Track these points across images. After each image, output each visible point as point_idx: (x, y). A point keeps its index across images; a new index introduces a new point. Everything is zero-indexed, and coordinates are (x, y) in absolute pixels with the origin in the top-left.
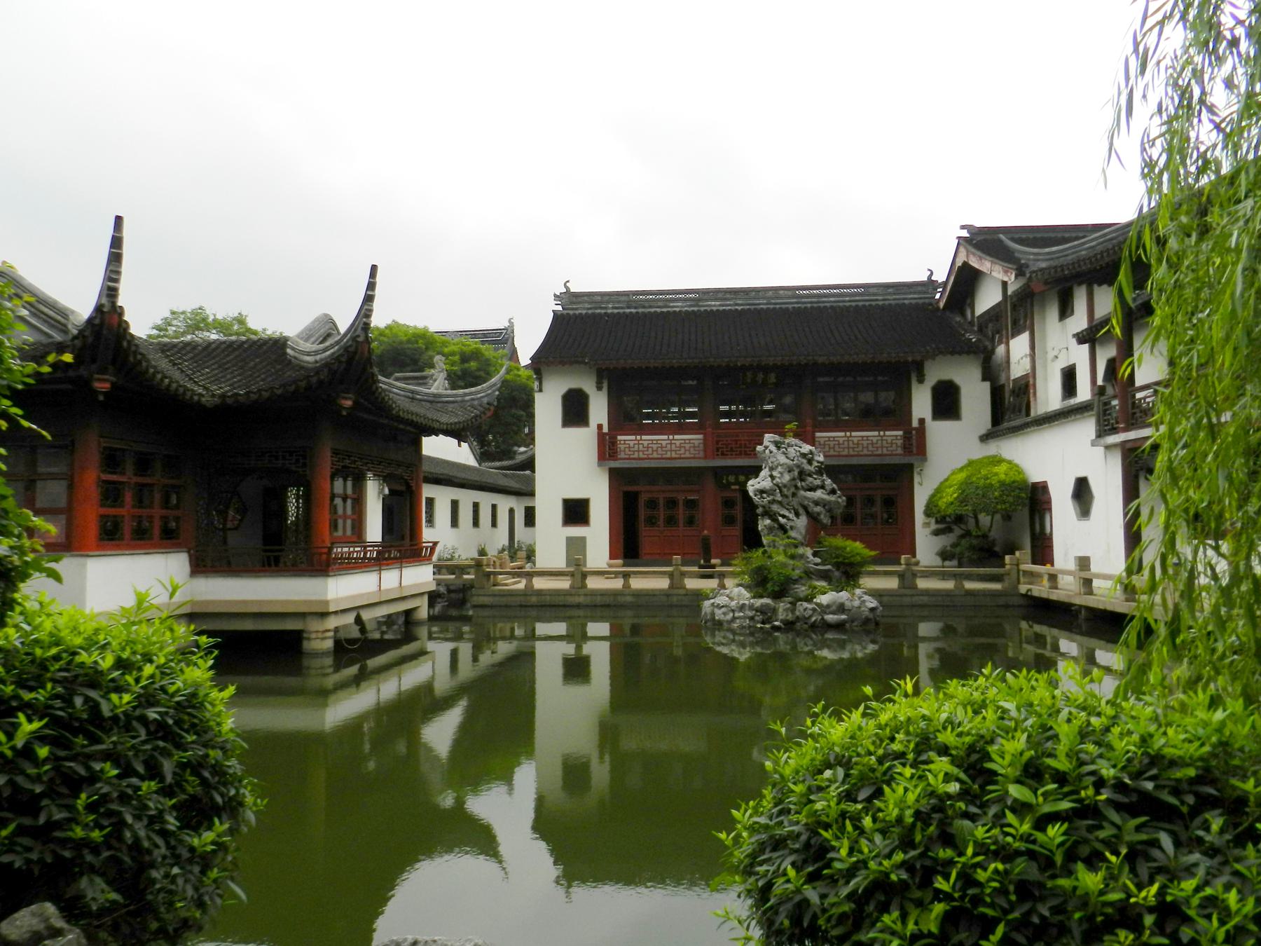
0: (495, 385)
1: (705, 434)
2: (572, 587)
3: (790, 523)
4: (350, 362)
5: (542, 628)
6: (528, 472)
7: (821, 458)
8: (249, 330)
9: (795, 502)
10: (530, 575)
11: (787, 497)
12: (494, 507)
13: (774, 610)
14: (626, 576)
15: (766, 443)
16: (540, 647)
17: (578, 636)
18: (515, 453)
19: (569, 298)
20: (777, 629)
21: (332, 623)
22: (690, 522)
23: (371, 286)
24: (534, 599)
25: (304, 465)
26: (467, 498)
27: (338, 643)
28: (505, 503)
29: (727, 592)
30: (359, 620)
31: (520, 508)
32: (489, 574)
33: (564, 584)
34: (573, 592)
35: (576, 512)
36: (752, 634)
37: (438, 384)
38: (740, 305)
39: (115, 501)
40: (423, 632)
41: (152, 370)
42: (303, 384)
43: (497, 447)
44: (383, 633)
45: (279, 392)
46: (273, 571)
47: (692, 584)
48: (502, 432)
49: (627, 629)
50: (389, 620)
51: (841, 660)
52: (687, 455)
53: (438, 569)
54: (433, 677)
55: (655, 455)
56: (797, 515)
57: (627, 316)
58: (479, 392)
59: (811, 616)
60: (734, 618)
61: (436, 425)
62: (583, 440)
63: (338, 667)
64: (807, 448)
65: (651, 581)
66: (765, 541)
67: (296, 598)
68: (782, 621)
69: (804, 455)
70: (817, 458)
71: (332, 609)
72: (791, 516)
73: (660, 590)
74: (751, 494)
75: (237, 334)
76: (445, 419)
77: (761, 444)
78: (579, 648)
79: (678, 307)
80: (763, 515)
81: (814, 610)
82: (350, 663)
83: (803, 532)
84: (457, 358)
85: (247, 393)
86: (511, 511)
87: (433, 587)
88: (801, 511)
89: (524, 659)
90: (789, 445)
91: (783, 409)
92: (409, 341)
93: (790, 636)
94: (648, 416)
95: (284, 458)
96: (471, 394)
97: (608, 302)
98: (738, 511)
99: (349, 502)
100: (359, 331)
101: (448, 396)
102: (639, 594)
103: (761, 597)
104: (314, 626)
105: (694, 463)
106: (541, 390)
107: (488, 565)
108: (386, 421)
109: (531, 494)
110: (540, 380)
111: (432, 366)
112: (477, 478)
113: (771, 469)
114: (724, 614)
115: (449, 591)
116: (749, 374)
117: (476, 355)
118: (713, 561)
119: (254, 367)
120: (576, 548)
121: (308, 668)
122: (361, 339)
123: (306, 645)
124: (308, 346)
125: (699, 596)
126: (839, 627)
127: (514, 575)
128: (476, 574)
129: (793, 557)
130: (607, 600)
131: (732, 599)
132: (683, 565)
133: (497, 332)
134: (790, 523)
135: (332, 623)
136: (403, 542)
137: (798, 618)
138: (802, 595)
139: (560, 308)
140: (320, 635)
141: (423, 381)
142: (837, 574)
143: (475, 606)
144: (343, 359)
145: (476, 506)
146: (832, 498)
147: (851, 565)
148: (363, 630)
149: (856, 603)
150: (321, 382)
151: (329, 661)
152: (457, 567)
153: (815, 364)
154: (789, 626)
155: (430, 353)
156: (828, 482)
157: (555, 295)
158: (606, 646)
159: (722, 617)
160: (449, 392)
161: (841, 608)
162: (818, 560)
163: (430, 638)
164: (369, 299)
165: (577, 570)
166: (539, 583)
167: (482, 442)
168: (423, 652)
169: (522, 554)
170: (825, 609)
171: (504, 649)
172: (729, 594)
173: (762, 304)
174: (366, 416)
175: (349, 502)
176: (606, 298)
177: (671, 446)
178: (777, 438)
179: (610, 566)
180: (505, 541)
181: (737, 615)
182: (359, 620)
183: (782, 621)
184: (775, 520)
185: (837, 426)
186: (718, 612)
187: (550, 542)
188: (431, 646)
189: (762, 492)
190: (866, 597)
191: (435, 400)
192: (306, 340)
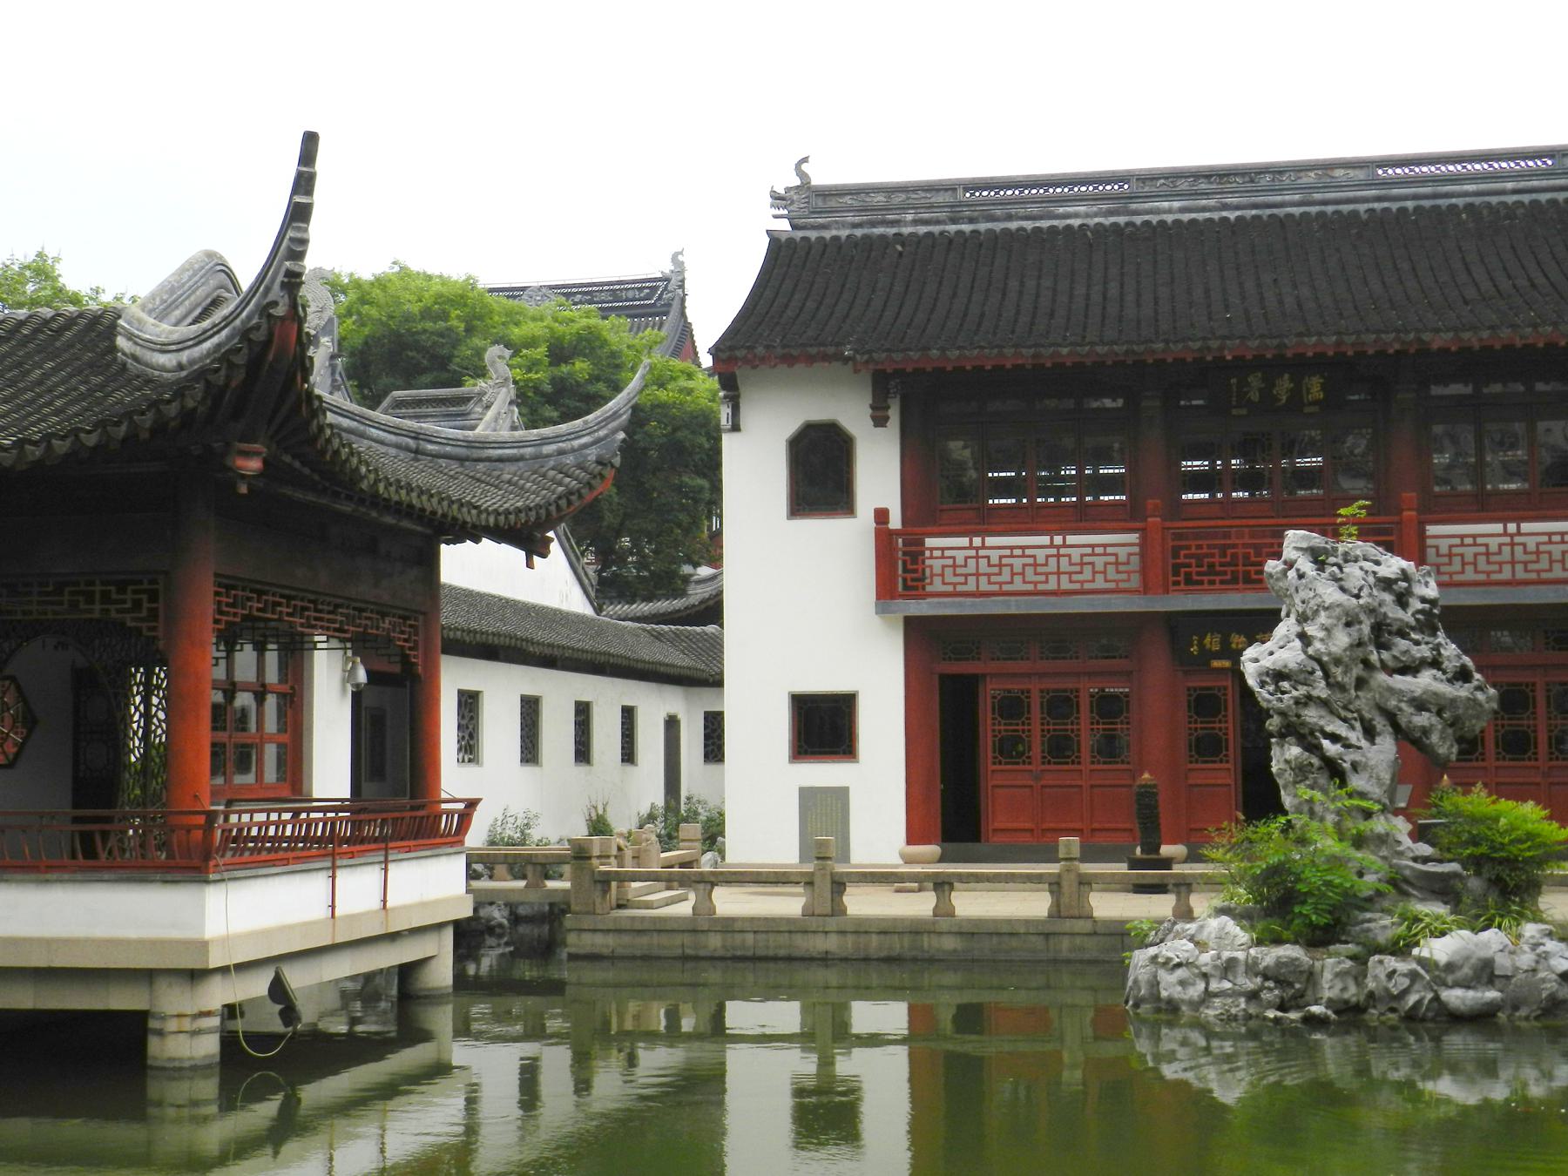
0: (615, 415)
1: (1143, 531)
2: (808, 912)
3: (1351, 756)
4: (255, 364)
5: (741, 1015)
6: (711, 629)
7: (1432, 591)
8: (59, 291)
9: (1363, 701)
10: (710, 882)
11: (1342, 688)
12: (628, 714)
13: (1311, 977)
14: (942, 885)
15: (1289, 552)
16: (740, 1063)
17: (829, 1033)
18: (686, 579)
19: (806, 198)
20: (1313, 1022)
21: (217, 995)
22: (1109, 748)
23: (304, 183)
24: (715, 942)
25: (153, 615)
26: (559, 692)
27: (229, 1042)
28: (655, 705)
29: (1192, 927)
30: (278, 990)
31: (689, 710)
32: (604, 881)
33: (789, 905)
34: (814, 923)
35: (823, 726)
36: (1253, 1035)
37: (495, 418)
38: (1233, 207)
39: (1068, 699)
40: (442, 1019)
41: (355, 460)
42: (147, 420)
43: (641, 565)
44: (354, 1021)
45: (91, 440)
46: (82, 869)
47: (1108, 906)
48: (645, 522)
49: (946, 1017)
50: (366, 988)
51: (1486, 1105)
52: (1100, 583)
53: (479, 867)
54: (471, 1130)
55: (1018, 585)
56: (1370, 733)
57: (950, 241)
58: (577, 435)
59: (1405, 992)
60: (1208, 995)
61: (469, 517)
62: (842, 548)
63: (228, 1103)
64: (1393, 565)
65: (1005, 899)
66: (1287, 800)
67: (133, 934)
68: (1330, 1003)
69: (1386, 584)
70: (1420, 590)
71: (213, 963)
72: (1355, 736)
73: (1027, 922)
74: (1252, 682)
75: (34, 302)
76: (492, 500)
77: (1277, 555)
78: (826, 1063)
79: (1079, 215)
80: (1282, 736)
81: (1413, 976)
82: (257, 1095)
83: (1386, 777)
84: (541, 352)
85: (20, 444)
86: (672, 724)
87: (466, 911)
88: (1380, 723)
89: (701, 1088)
90: (1347, 558)
91: (1340, 464)
92: (426, 314)
93: (1350, 1040)
94: (1003, 488)
95: (106, 597)
96: (557, 438)
97: (903, 208)
98: (1230, 725)
99: (271, 701)
100: (276, 293)
101: (502, 444)
102: (976, 931)
103: (1278, 941)
104: (172, 1001)
105: (1119, 604)
106: (736, 428)
107: (604, 857)
108: (347, 508)
109: (718, 683)
110: (735, 402)
111: (481, 372)
112: (587, 645)
113: (1303, 619)
114: (1183, 983)
115: (515, 919)
116: (1255, 380)
117: (588, 344)
118: (1166, 850)
119: (40, 383)
120: (824, 815)
121: (159, 1104)
122: (280, 311)
123: (154, 1045)
124: (164, 330)
125: (1122, 937)
126: (1480, 1019)
127: (669, 881)
128: (575, 879)
129: (1359, 842)
130: (897, 945)
131: (1201, 946)
132: (1086, 857)
133: (649, 287)
134: (1351, 756)
135: (217, 995)
136: (399, 802)
137: (1371, 995)
138: (1382, 939)
139: (784, 225)
140: (187, 1025)
141: (457, 408)
142: (1475, 884)
143: (573, 957)
144: (240, 360)
145: (583, 712)
146: (1462, 691)
147: (1511, 862)
148: (289, 1013)
149: (1526, 959)
150: (187, 417)
151: (208, 1088)
152: (530, 860)
153: (1424, 352)
154: (1350, 1014)
155: (477, 341)
156: (1450, 650)
157: (776, 197)
158: (898, 1058)
159: (1177, 992)
160: (520, 434)
161: (1485, 972)
162: (1425, 849)
163: (463, 1030)
164: (298, 214)
165: (825, 871)
166: (730, 903)
167: (607, 555)
168: (440, 1070)
169: (692, 830)
170: (1443, 973)
171: (657, 1061)
172: (1194, 935)
173: (1290, 204)
174: (299, 495)
175: (271, 701)
176: (899, 199)
177: (1059, 563)
178: (1317, 540)
179: (908, 860)
180: (655, 795)
181: (1215, 986)
182: (278, 990)
183: (1330, 1003)
184: (1314, 748)
185: (1483, 506)
186: (1163, 975)
187: (761, 799)
188: (461, 1053)
189: (1279, 675)
190: (1551, 945)
191: (470, 456)
192: (161, 317)
